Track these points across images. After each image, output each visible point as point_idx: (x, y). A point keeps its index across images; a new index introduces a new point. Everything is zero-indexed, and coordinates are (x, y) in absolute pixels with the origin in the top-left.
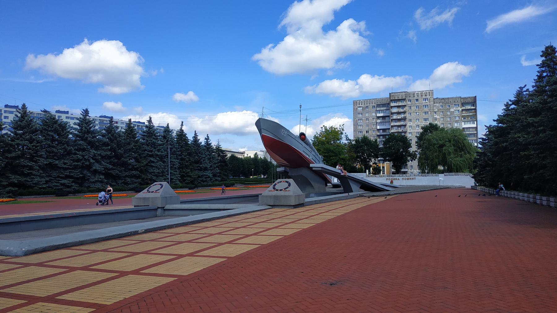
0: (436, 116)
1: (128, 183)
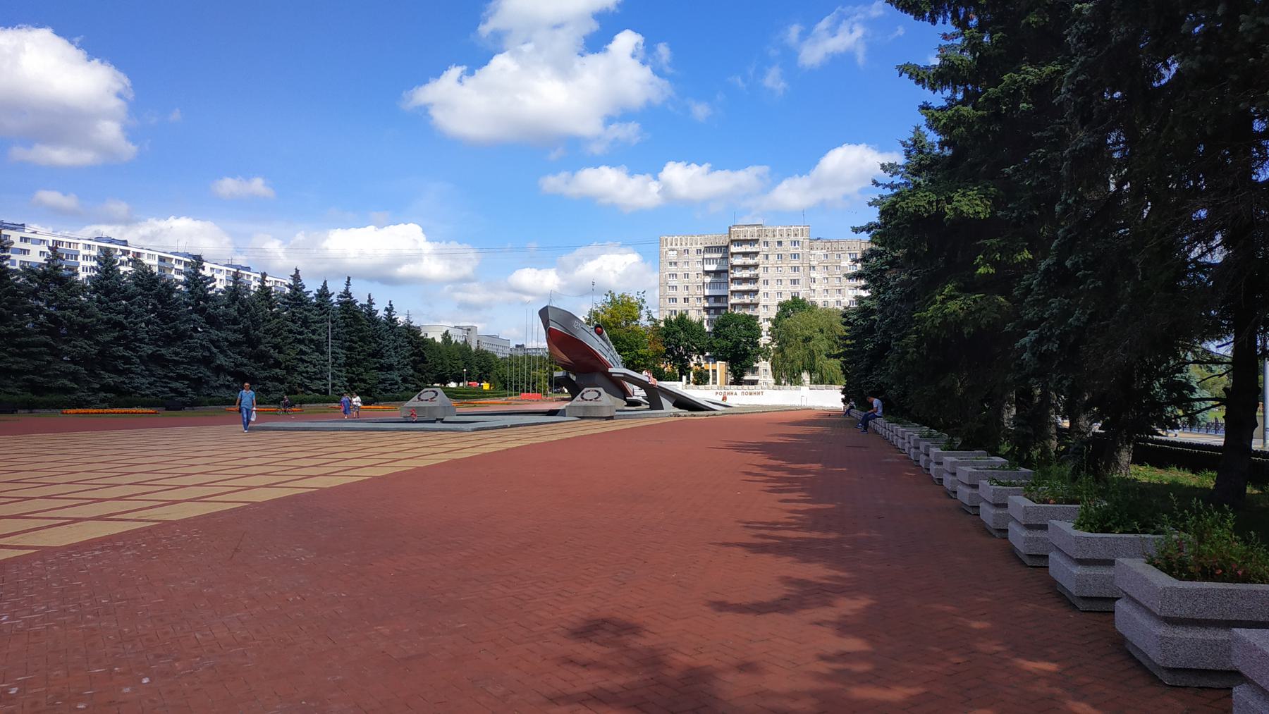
0: (814, 274)
1: (269, 391)
